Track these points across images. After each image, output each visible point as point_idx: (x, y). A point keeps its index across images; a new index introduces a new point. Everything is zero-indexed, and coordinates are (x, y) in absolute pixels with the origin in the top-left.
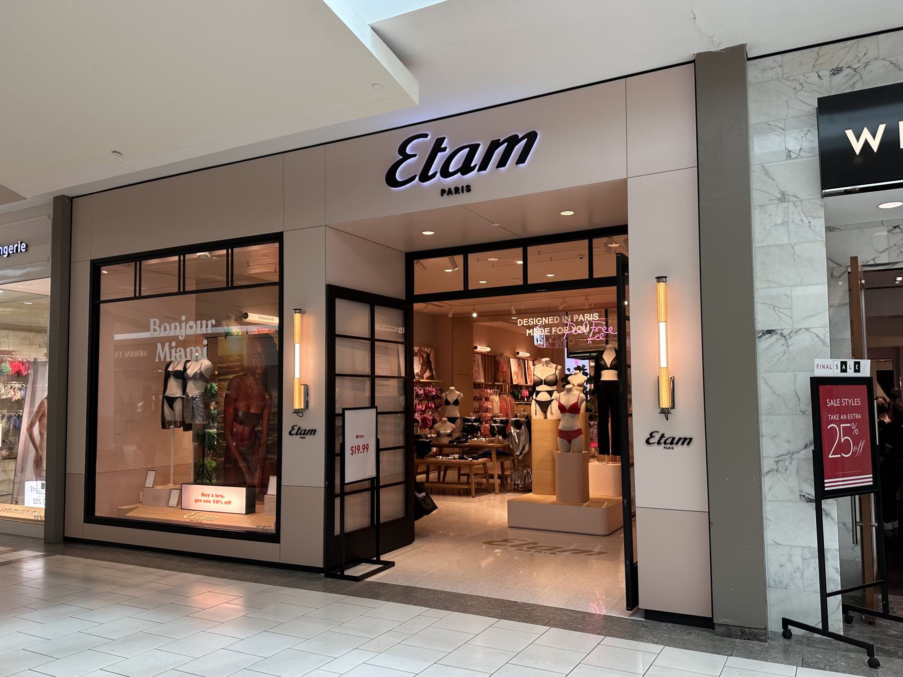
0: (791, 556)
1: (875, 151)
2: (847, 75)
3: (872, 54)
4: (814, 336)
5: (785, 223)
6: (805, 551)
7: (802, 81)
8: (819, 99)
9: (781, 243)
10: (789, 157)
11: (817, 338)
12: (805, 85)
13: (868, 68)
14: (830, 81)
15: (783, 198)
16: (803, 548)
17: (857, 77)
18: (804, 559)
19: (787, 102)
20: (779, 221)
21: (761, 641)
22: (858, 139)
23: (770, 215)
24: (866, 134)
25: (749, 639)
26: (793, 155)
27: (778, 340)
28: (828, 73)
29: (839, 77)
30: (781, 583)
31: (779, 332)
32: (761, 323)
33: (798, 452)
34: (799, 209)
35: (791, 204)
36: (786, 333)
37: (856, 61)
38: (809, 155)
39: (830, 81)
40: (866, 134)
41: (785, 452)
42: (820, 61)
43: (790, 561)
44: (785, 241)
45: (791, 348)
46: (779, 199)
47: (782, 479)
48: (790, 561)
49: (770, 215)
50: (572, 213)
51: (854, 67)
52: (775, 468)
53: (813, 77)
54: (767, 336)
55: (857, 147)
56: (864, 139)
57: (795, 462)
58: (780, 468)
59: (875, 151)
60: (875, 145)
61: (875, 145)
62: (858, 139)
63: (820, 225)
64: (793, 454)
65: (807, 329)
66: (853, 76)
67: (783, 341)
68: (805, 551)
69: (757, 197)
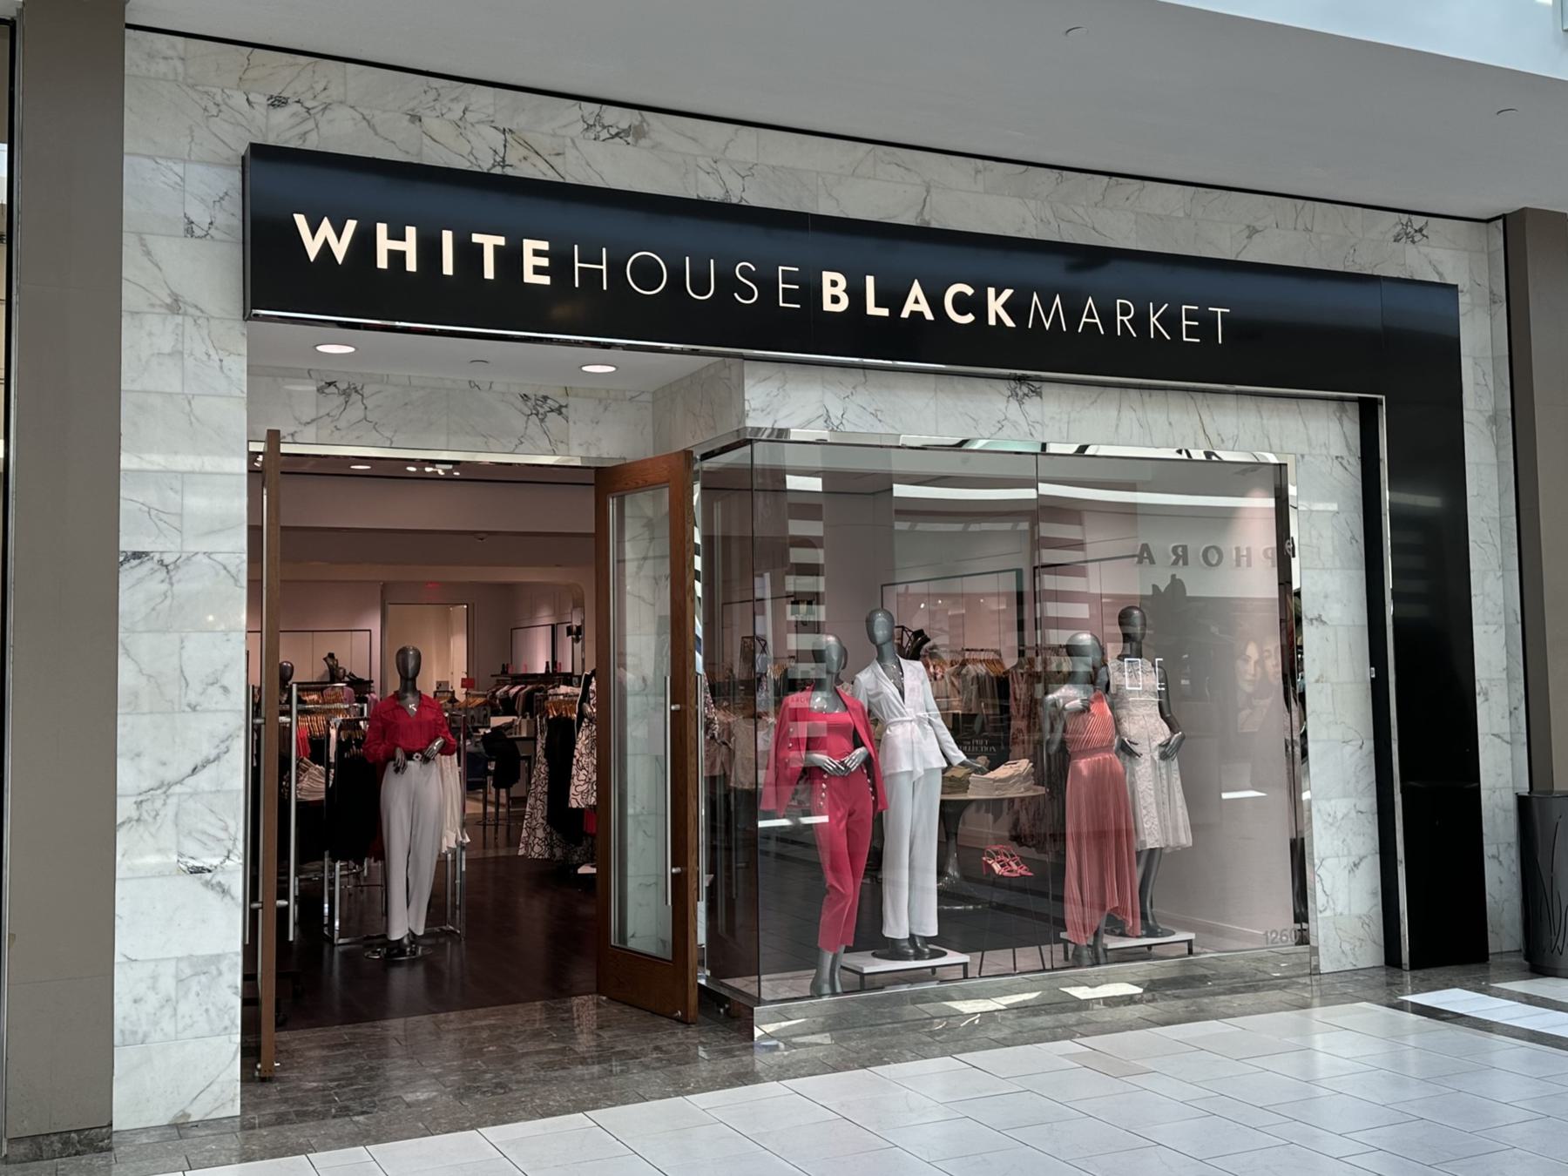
0: (155, 978)
1: (312, 259)
2: (294, 114)
3: (335, 92)
4: (219, 567)
5: (177, 354)
6: (183, 965)
7: (219, 99)
8: (253, 146)
9: (168, 390)
10: (189, 232)
11: (223, 572)
12: (223, 107)
13: (329, 114)
14: (267, 117)
15: (175, 306)
16: (178, 959)
17: (310, 124)
18: (180, 981)
19: (190, 128)
20: (167, 349)
21: (102, 1150)
22: (314, 234)
23: (150, 334)
24: (326, 228)
25: (78, 1153)
26: (198, 232)
27: (153, 571)
28: (263, 100)
29: (281, 116)
30: (134, 1033)
31: (157, 557)
32: (127, 544)
33: (181, 782)
34: (205, 332)
35: (189, 321)
36: (168, 559)
37: (310, 95)
38: (225, 237)
39: (267, 117)
40: (326, 228)
41: (154, 784)
42: (251, 74)
43: (153, 988)
44: (176, 387)
45: (176, 587)
46: (168, 306)
47: (146, 835)
48: (153, 988)
49: (150, 334)
50: (351, 350)
51: (309, 104)
52: (135, 815)
53: (239, 99)
54: (134, 562)
55: (313, 248)
56: (324, 239)
57: (173, 801)
58: (145, 816)
59: (312, 259)
60: (340, 250)
61: (340, 250)
62: (314, 234)
63: (238, 367)
64: (170, 786)
65: (208, 554)
66: (305, 120)
67: (162, 574)
68: (183, 965)
69: (130, 296)
